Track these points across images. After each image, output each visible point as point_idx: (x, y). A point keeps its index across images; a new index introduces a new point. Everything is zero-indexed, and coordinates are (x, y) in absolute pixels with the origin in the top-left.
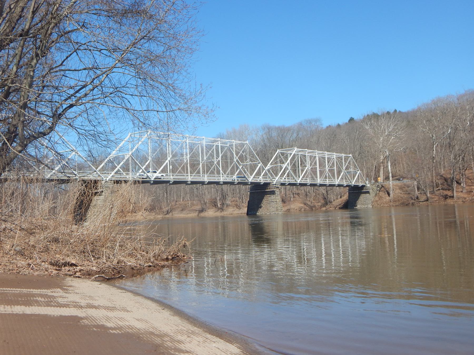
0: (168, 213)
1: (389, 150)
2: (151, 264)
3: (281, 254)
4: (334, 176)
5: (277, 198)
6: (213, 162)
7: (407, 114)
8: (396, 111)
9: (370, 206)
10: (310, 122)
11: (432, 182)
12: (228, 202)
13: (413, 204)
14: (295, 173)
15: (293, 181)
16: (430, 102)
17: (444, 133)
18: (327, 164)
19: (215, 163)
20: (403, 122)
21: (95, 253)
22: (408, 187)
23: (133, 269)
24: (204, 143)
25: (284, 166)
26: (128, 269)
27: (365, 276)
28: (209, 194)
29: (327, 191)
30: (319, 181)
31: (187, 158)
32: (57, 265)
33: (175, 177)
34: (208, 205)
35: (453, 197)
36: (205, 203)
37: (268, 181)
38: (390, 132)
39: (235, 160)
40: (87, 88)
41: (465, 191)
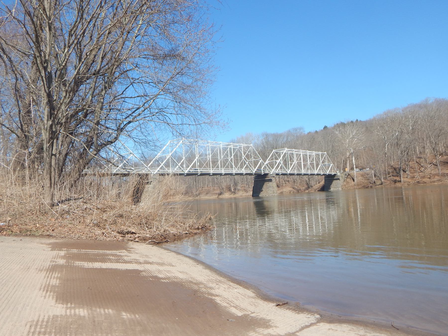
3: (277, 223)
5: (273, 184)
7: (366, 122)
8: (357, 120)
9: (340, 189)
10: (296, 129)
11: (385, 171)
13: (371, 187)
17: (393, 135)
19: (229, 160)
22: (368, 175)
23: (174, 235)
25: (278, 161)
27: (337, 240)
30: (303, 171)
34: (224, 190)
35: (400, 181)
36: (223, 189)
38: (353, 136)
39: (243, 158)
40: (140, 110)
41: (409, 177)
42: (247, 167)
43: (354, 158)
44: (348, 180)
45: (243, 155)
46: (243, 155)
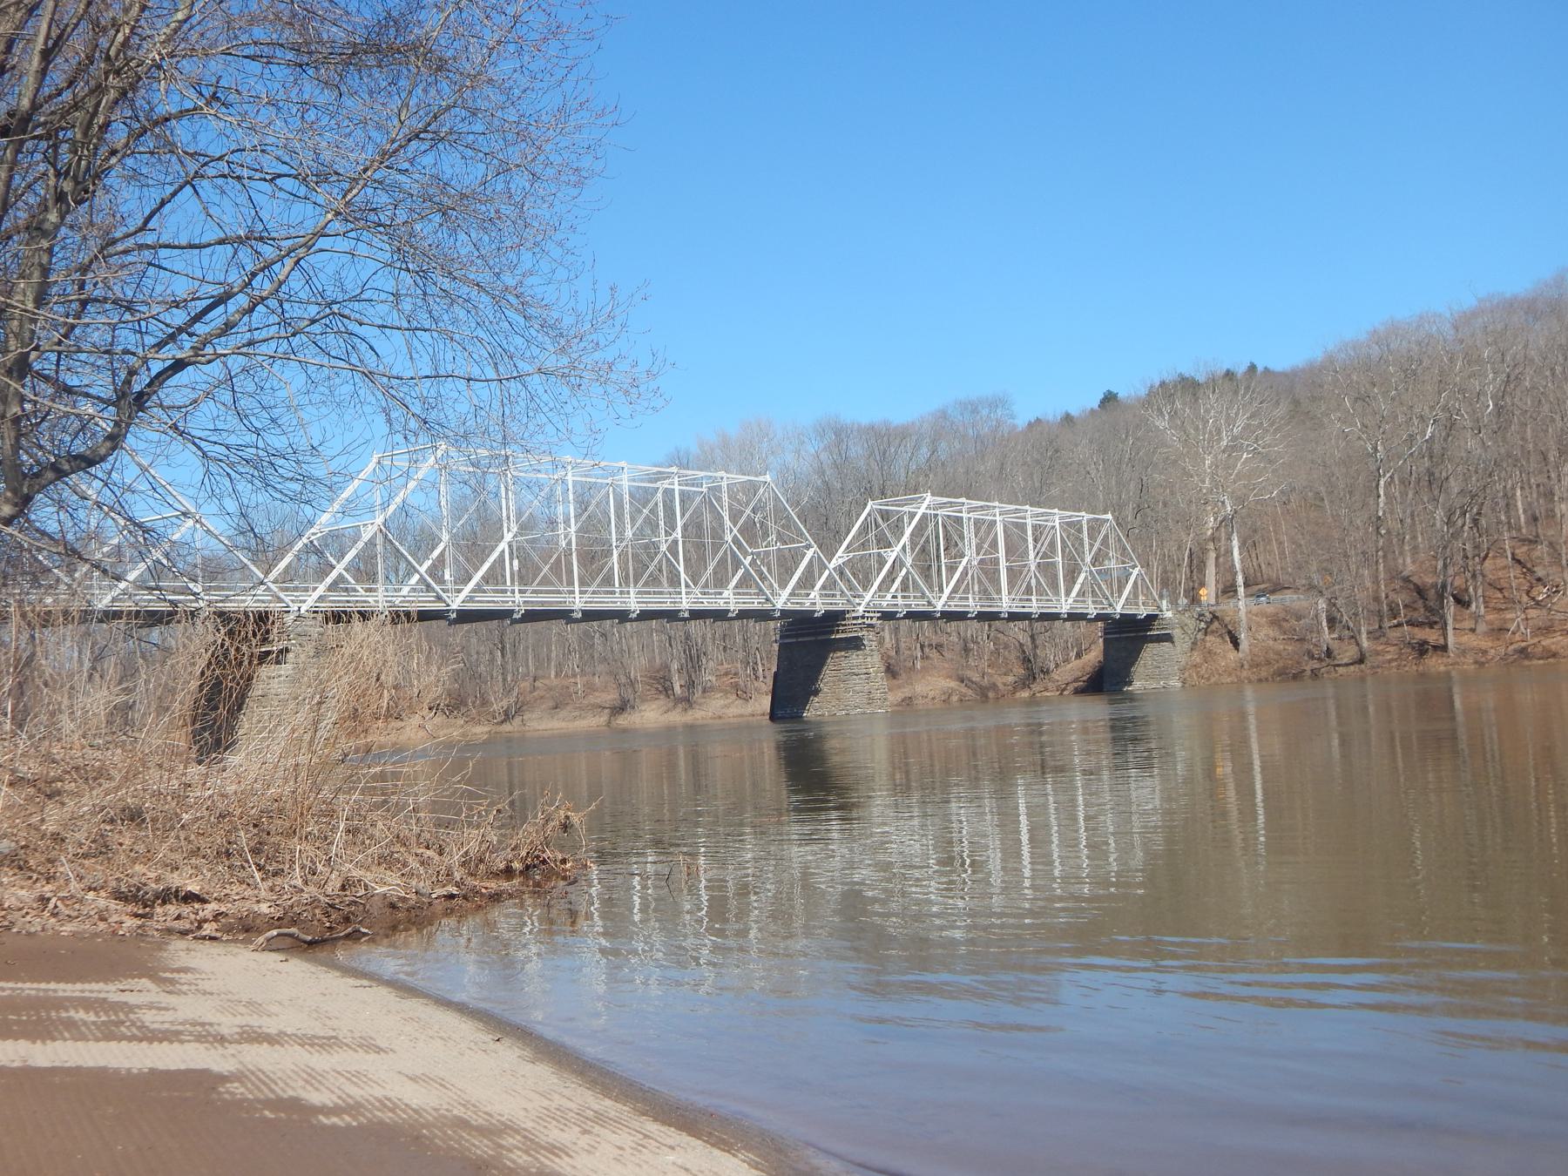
0: (508, 716)
1: (1232, 495)
2: (454, 890)
3: (891, 840)
4: (1054, 586)
5: (868, 662)
7: (1291, 377)
8: (1252, 368)
9: (1175, 683)
10: (973, 407)
11: (1377, 599)
12: (708, 677)
13: (1315, 674)
14: (927, 577)
15: (918, 605)
17: (1412, 438)
18: (1031, 547)
19: (664, 548)
20: (1278, 403)
23: (393, 906)
25: (891, 555)
26: (376, 908)
27: (1157, 913)
28: (642, 651)
29: (1032, 637)
30: (1006, 603)
31: (569, 534)
32: (138, 899)
33: (530, 597)
34: (640, 687)
35: (1444, 648)
36: (632, 684)
37: (839, 604)
38: (1234, 439)
39: (729, 538)
40: (232, 306)
41: (1482, 627)
42: (745, 581)
43: (1235, 543)
45: (728, 523)
46: (728, 523)
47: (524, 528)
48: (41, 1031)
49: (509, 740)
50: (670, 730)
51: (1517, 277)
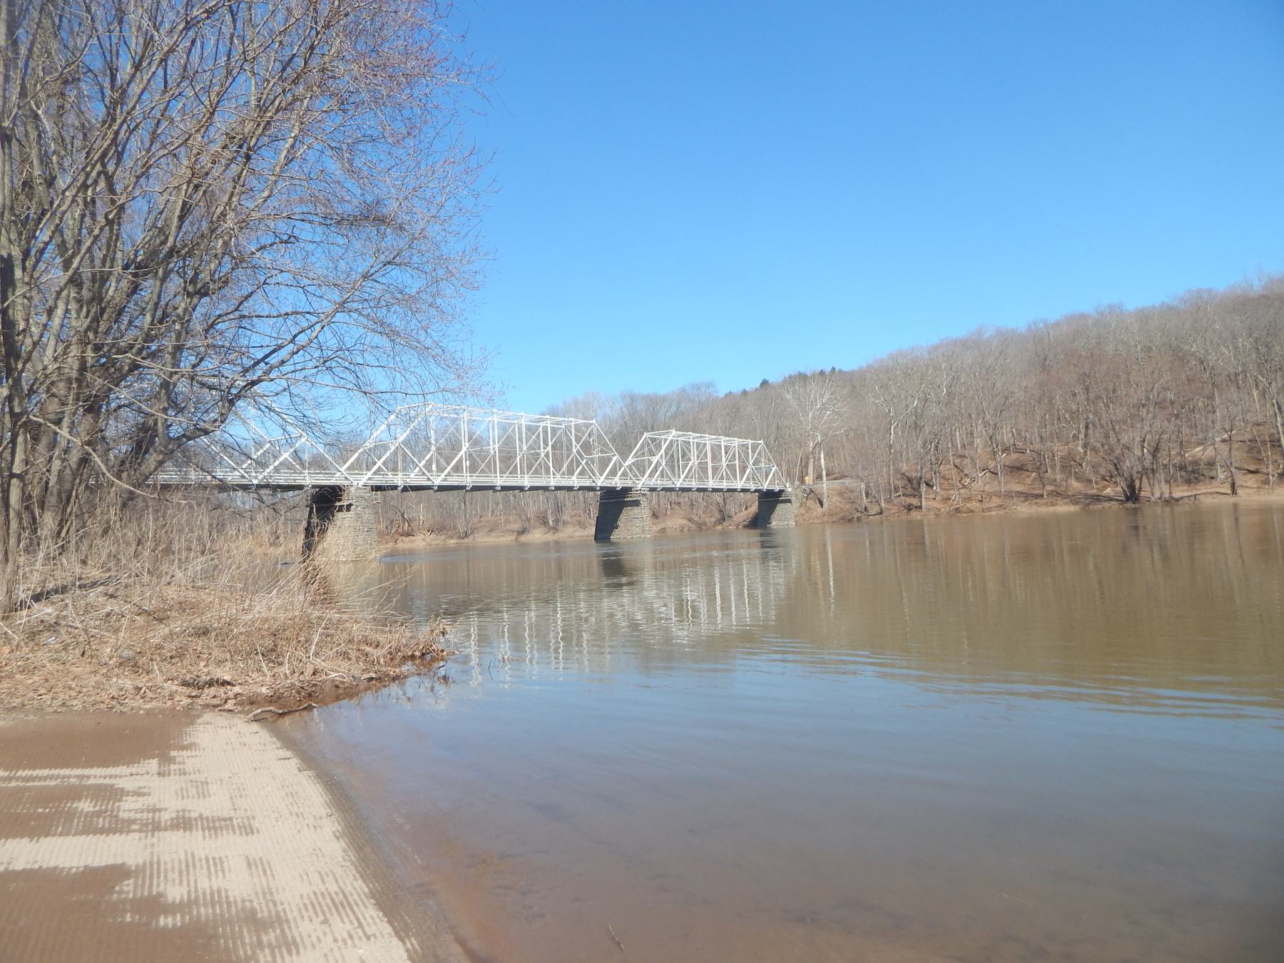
0: (466, 535)
1: (822, 433)
3: (650, 599)
5: (643, 512)
6: (538, 454)
7: (852, 373)
8: (834, 369)
10: (697, 387)
12: (566, 518)
13: (859, 519)
14: (673, 471)
16: (885, 356)
17: (907, 406)
21: (272, 655)
23: (337, 686)
24: (523, 422)
25: (655, 460)
27: (791, 626)
28: (533, 505)
30: (711, 484)
31: (494, 448)
32: (194, 684)
33: (474, 479)
35: (920, 507)
37: (629, 484)
39: (574, 451)
41: (938, 498)
42: (582, 473)
44: (810, 503)
45: (574, 443)
46: (574, 443)
47: (473, 445)
48: (36, 827)
49: (468, 548)
50: (547, 544)
51: (959, 330)
